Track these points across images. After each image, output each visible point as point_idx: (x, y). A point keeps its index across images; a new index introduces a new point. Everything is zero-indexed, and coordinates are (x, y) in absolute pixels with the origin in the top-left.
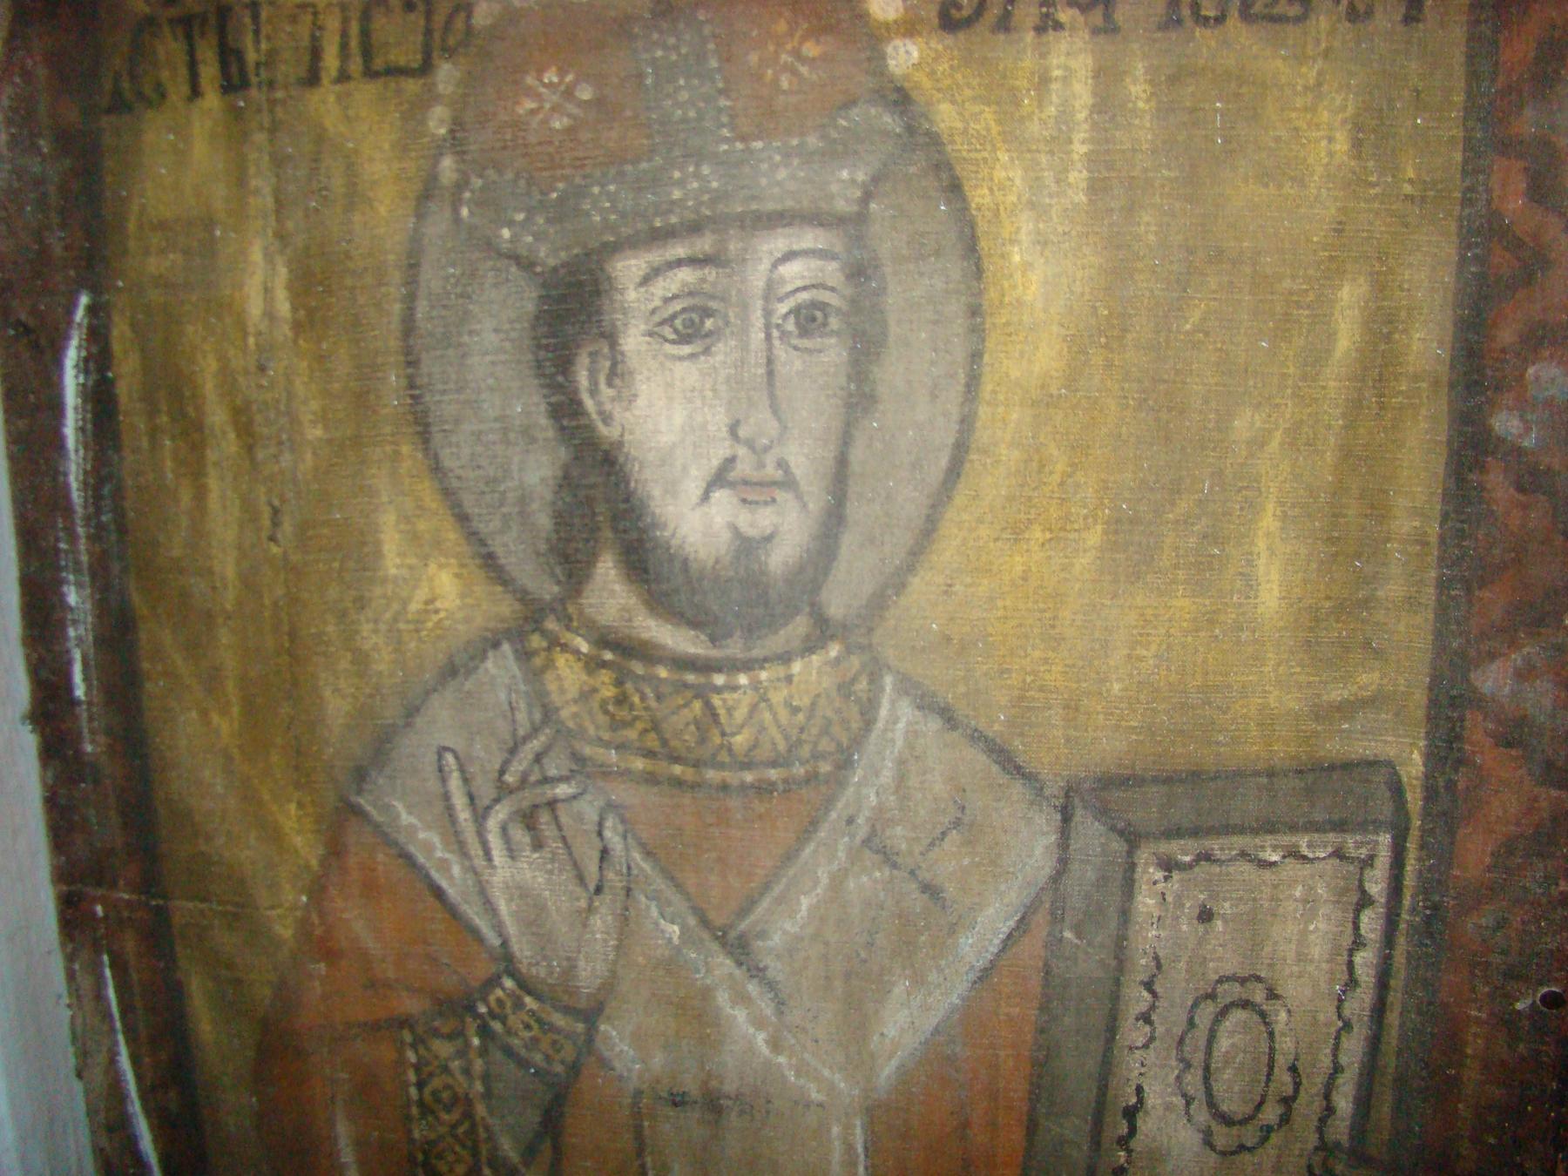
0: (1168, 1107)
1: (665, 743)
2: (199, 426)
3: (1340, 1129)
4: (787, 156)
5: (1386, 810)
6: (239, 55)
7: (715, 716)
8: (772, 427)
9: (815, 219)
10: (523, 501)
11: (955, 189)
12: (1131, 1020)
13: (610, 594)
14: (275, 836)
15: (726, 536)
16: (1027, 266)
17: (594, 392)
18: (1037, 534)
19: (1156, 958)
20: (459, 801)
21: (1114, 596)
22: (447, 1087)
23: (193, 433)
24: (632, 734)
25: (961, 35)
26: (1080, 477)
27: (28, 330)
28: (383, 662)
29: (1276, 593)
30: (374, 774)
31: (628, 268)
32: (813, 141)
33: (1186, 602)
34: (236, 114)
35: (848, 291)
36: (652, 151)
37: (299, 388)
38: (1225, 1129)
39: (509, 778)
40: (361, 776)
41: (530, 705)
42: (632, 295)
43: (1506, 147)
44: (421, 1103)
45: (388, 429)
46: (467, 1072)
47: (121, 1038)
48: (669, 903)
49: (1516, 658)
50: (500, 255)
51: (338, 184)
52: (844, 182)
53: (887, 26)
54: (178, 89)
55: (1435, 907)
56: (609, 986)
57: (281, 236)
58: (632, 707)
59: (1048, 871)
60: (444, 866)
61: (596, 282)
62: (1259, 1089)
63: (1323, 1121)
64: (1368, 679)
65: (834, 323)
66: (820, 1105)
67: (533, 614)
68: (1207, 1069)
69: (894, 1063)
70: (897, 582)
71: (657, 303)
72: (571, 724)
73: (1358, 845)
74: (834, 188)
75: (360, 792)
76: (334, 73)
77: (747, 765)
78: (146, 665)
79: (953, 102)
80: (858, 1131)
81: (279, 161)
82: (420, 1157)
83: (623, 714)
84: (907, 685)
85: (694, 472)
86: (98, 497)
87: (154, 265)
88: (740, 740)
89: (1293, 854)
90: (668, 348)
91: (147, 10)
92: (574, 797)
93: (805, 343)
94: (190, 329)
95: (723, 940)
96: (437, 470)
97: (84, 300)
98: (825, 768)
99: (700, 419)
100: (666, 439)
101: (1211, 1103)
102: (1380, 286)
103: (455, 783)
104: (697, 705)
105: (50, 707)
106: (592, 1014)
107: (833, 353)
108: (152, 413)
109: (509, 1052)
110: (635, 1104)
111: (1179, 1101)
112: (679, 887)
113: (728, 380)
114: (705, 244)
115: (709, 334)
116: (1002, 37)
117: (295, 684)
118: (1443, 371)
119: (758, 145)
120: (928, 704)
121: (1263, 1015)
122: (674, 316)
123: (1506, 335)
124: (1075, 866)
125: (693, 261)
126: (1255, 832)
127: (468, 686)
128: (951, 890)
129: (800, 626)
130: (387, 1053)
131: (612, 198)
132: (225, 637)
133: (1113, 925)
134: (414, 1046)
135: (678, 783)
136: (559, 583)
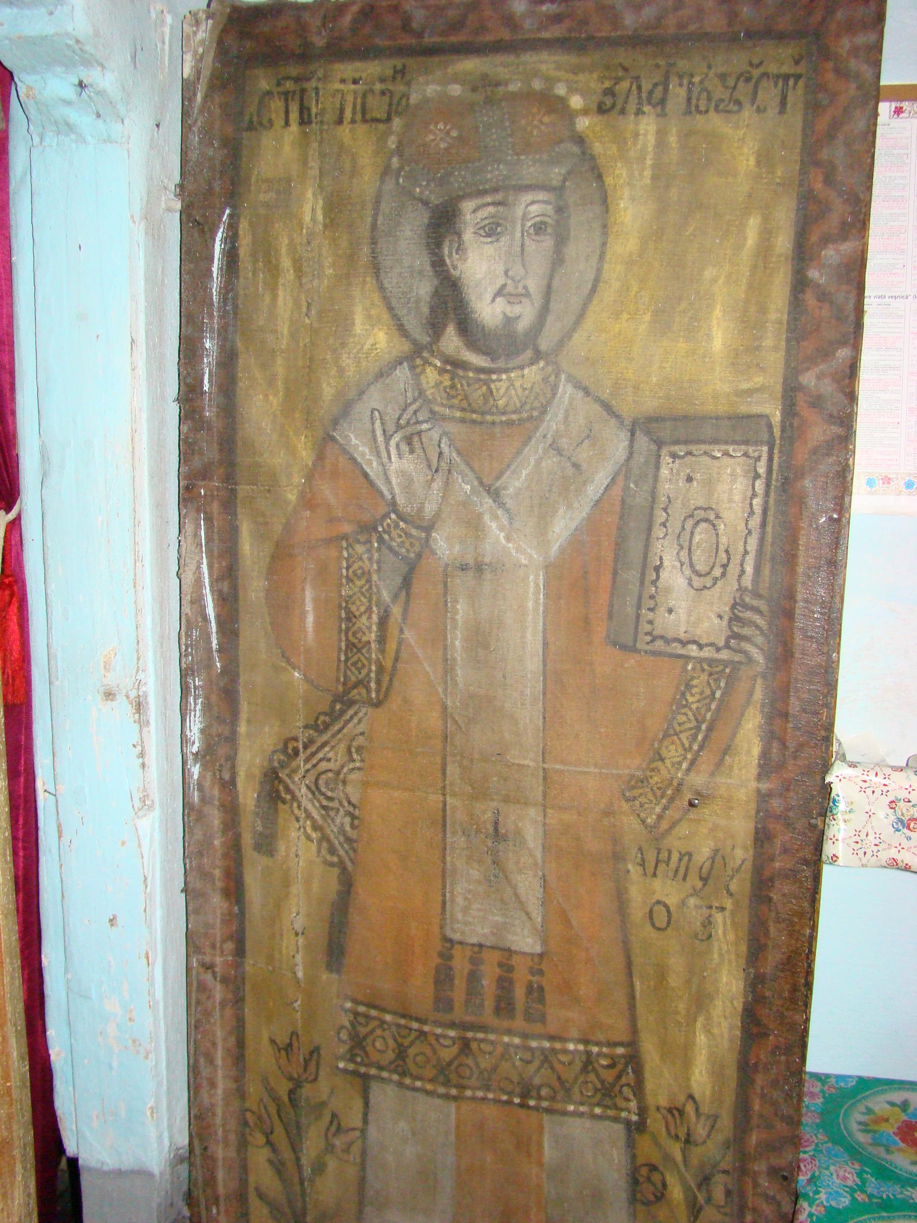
0: (674, 567)
1: (470, 405)
2: (277, 267)
3: (747, 581)
4: (534, 162)
5: (765, 437)
6: (309, 110)
7: (491, 392)
8: (522, 272)
9: (543, 187)
10: (418, 301)
11: (600, 177)
12: (658, 526)
13: (451, 341)
14: (292, 451)
15: (501, 316)
16: (626, 209)
17: (450, 256)
18: (625, 316)
19: (668, 497)
20: (379, 432)
21: (655, 342)
22: (360, 568)
23: (273, 270)
24: (455, 401)
25: (606, 116)
26: (643, 293)
27: (199, 223)
28: (351, 372)
29: (720, 342)
30: (341, 421)
31: (468, 206)
32: (545, 157)
33: (683, 345)
34: (305, 135)
35: (556, 217)
36: (480, 159)
37: (324, 252)
38: (697, 578)
39: (402, 422)
40: (335, 422)
41: (413, 390)
42: (468, 217)
43: (817, 164)
44: (347, 577)
45: (362, 271)
46: (370, 559)
47: (204, 555)
48: (467, 475)
49: (817, 370)
50: (415, 198)
51: (348, 166)
52: (556, 173)
53: (576, 110)
54: (279, 122)
55: (786, 478)
56: (438, 514)
57: (321, 187)
58: (457, 390)
59: (624, 457)
60: (370, 462)
61: (454, 211)
62: (712, 560)
63: (740, 576)
64: (759, 380)
65: (549, 230)
66: (526, 566)
67: (418, 350)
68: (690, 550)
69: (558, 544)
70: (568, 335)
71: (478, 220)
72: (430, 397)
73: (754, 451)
74: (552, 176)
75: (334, 430)
76: (349, 120)
77: (504, 413)
78: (240, 375)
79: (601, 142)
80: (541, 577)
81: (323, 156)
82: (344, 605)
83: (453, 393)
84: (570, 378)
85: (489, 290)
86: (225, 300)
87: (262, 197)
88: (501, 403)
89: (726, 454)
90: (482, 239)
91: (268, 88)
92: (429, 430)
93: (537, 238)
94: (277, 225)
95: (488, 492)
96: (382, 288)
97: (228, 211)
98: (535, 414)
99: (493, 268)
100: (479, 276)
101: (692, 565)
102: (766, 219)
103: (378, 424)
104: (484, 388)
105: (189, 394)
106: (428, 529)
107: (548, 242)
108: (256, 261)
109: (390, 549)
110: (445, 570)
111: (679, 565)
112: (472, 469)
113: (506, 251)
114: (499, 197)
115: (499, 233)
116: (621, 116)
117: (310, 381)
118: (790, 253)
119: (523, 157)
120: (579, 386)
121: (714, 525)
122: (484, 227)
123: (814, 238)
124: (635, 455)
125: (494, 204)
126: (710, 443)
127: (387, 381)
128: (584, 466)
129: (529, 354)
130: (334, 553)
131: (464, 178)
132: (279, 361)
133: (651, 481)
134: (347, 549)
135: (474, 422)
136: (430, 336)
